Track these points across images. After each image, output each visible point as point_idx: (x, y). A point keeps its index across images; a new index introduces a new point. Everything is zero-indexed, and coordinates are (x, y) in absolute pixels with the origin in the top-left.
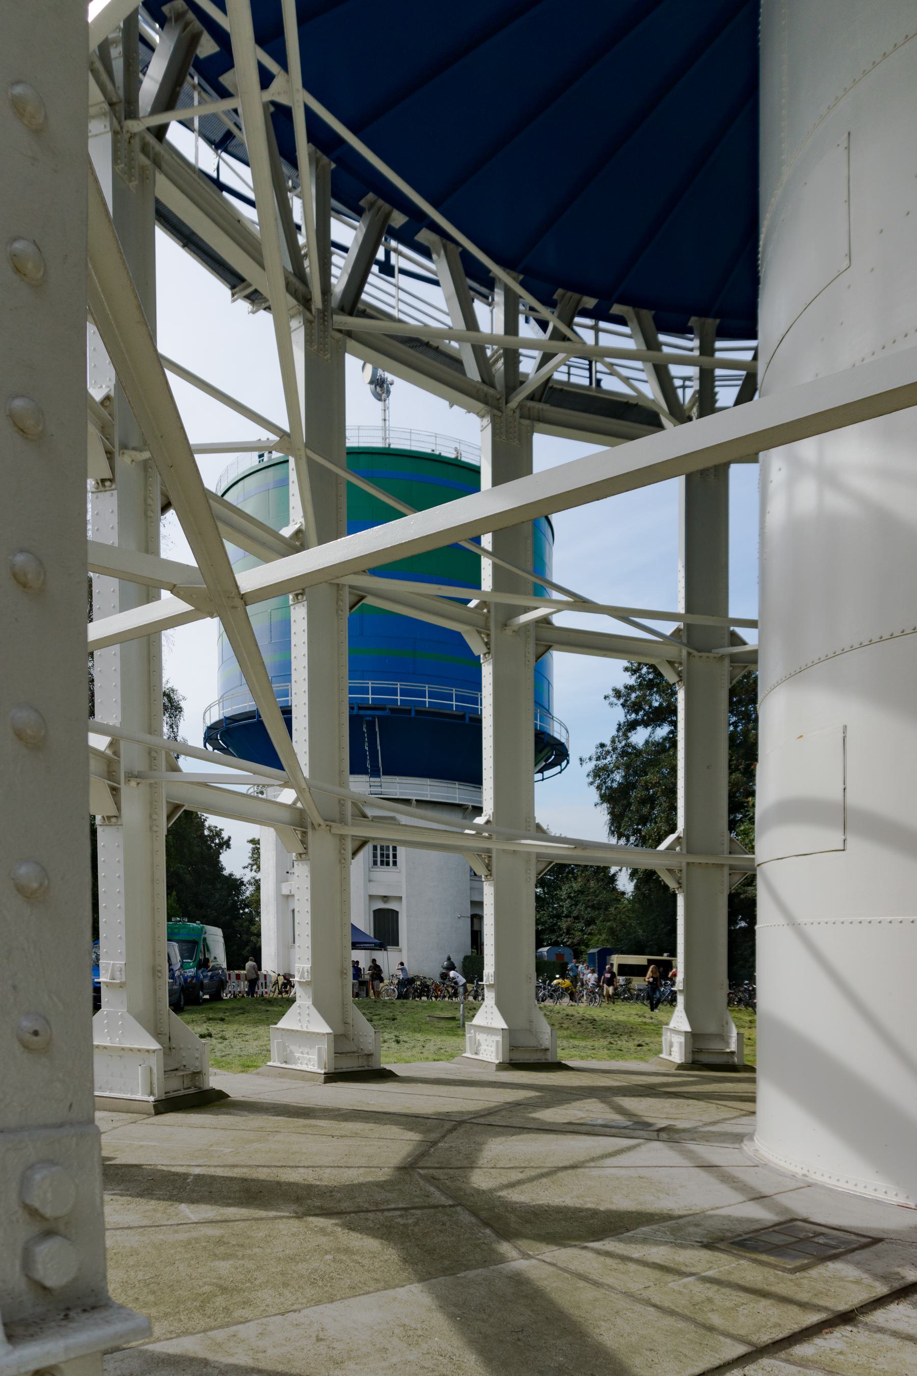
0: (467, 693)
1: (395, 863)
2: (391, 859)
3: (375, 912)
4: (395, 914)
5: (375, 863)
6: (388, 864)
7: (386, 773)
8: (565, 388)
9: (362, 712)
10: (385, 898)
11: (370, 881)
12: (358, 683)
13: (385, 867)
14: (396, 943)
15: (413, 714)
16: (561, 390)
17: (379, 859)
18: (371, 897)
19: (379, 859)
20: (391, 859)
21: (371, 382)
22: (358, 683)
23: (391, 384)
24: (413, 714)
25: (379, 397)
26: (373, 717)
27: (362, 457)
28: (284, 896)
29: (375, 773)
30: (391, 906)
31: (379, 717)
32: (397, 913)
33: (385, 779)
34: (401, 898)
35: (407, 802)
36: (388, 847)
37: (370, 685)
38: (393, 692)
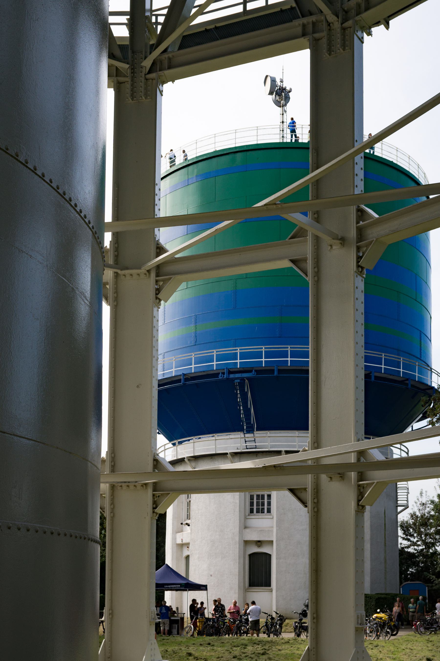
0: (299, 348)
1: (269, 511)
2: (266, 507)
3: (252, 556)
4: (268, 557)
5: (252, 511)
6: (263, 512)
7: (259, 429)
8: (218, 25)
9: (232, 376)
10: (259, 543)
11: (246, 527)
12: (373, 354)
13: (260, 514)
14: (268, 584)
15: (276, 373)
16: (216, 28)
17: (255, 507)
18: (247, 543)
19: (255, 507)
20: (266, 507)
21: (271, 93)
22: (373, 354)
23: (290, 92)
24: (276, 373)
25: (277, 103)
26: (242, 379)
27: (238, 155)
28: (178, 545)
29: (250, 430)
30: (265, 550)
31: (248, 379)
32: (270, 556)
33: (258, 434)
34: (272, 541)
35: (287, 452)
36: (263, 496)
37: (263, 350)
38: (234, 357)
